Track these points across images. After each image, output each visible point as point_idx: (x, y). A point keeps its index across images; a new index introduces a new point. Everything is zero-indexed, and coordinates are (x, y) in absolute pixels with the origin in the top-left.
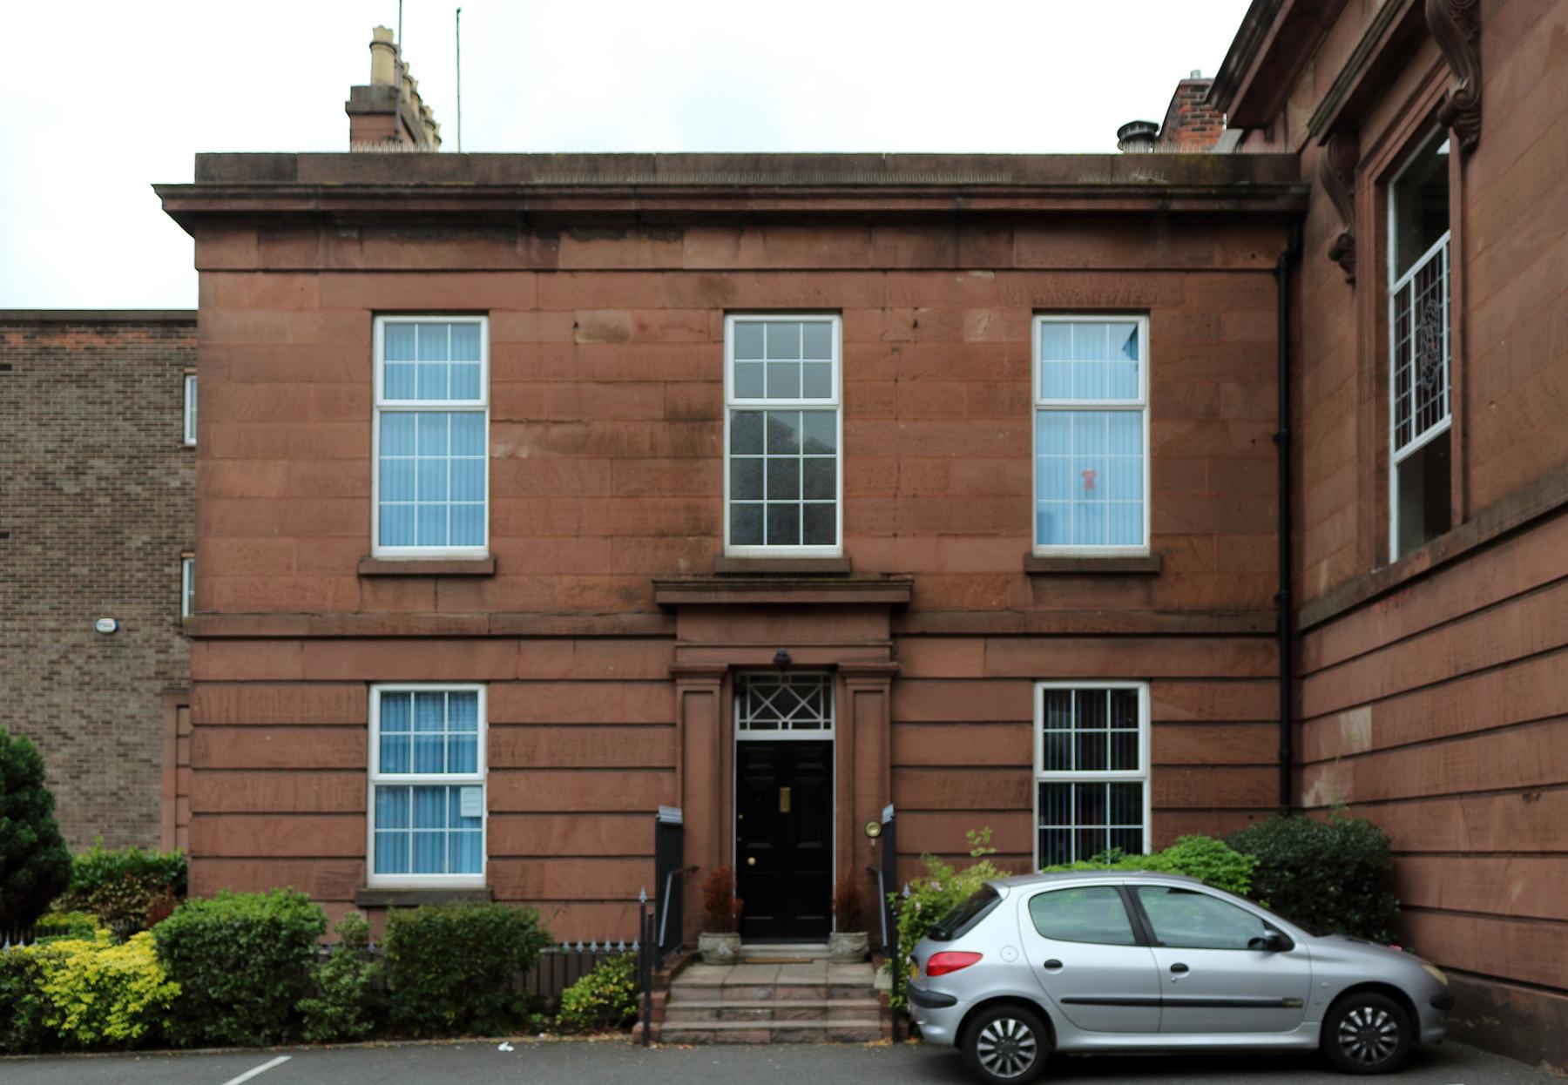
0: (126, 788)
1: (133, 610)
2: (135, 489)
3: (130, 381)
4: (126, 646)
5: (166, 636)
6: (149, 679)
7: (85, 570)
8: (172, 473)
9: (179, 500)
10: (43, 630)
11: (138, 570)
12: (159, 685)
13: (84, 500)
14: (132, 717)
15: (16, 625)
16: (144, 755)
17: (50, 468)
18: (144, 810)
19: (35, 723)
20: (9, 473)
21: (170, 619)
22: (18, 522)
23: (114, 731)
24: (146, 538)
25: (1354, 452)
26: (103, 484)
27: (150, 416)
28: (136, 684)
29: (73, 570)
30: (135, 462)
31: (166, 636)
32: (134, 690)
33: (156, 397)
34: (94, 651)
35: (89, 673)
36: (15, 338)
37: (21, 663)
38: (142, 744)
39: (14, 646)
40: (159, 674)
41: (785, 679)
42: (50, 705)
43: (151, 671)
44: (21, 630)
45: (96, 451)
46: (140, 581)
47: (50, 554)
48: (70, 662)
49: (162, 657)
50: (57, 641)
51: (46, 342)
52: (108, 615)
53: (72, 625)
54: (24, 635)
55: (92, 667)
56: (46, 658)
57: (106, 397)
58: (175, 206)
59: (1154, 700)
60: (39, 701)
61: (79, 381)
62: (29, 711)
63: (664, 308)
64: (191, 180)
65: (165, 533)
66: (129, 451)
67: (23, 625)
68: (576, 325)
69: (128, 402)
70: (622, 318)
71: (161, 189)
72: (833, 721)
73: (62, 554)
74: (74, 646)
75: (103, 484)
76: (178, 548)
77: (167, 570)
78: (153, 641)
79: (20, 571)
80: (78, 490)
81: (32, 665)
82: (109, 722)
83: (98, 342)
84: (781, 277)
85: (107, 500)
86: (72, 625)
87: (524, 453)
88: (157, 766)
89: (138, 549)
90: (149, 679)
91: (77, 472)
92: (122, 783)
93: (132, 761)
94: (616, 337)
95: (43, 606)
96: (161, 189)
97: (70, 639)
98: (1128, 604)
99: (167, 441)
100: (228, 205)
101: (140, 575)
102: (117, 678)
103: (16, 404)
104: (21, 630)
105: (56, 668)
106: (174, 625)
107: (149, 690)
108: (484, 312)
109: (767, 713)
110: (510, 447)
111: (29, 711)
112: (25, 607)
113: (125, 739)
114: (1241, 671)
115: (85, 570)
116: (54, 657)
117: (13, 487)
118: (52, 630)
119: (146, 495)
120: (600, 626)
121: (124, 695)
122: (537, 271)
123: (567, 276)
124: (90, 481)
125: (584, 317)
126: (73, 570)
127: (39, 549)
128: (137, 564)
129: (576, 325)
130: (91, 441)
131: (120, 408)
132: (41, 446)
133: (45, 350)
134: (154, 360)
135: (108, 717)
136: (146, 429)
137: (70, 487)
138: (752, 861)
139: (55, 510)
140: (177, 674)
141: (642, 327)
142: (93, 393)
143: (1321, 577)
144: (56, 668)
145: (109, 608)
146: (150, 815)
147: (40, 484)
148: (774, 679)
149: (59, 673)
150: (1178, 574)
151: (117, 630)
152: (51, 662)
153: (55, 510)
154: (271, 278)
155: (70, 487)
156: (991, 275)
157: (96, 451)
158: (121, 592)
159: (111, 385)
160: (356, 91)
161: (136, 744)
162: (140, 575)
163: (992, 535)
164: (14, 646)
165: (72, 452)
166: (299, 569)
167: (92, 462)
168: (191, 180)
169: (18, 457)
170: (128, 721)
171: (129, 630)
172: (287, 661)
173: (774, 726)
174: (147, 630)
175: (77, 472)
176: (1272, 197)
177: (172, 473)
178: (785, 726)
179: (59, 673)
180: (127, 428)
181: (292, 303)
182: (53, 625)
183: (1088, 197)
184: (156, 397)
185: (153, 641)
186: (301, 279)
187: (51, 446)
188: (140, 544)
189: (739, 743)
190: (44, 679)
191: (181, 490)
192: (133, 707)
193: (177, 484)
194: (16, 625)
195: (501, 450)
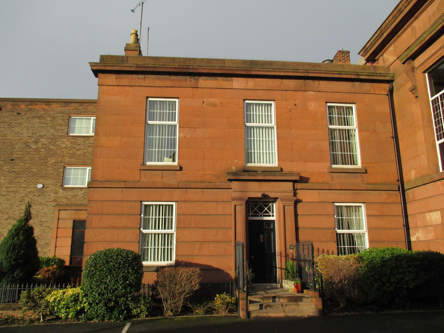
0: (41, 235)
1: (48, 182)
2: (52, 147)
3: (54, 118)
4: (45, 192)
5: (57, 189)
6: (51, 202)
7: (35, 170)
8: (63, 143)
9: (64, 150)
10: (21, 187)
11: (51, 170)
12: (54, 204)
13: (37, 150)
14: (45, 213)
15: (13, 186)
16: (47, 225)
17: (29, 141)
18: (46, 242)
19: (16, 215)
20: (16, 142)
21: (59, 184)
22: (17, 156)
23: (39, 217)
24: (54, 161)
25: (424, 140)
26: (43, 146)
27: (59, 127)
28: (47, 203)
29: (32, 170)
30: (53, 140)
31: (57, 189)
32: (46, 205)
33: (61, 122)
34: (35, 193)
35: (33, 200)
36: (23, 106)
37: (13, 197)
38: (47, 221)
39: (12, 192)
40: (54, 200)
41: (261, 202)
42: (21, 210)
43: (52, 200)
44: (15, 187)
45: (42, 137)
46: (51, 173)
47: (26, 165)
48: (28, 197)
49: (56, 195)
50: (25, 190)
51: (31, 107)
52: (41, 183)
53: (30, 186)
54: (15, 189)
55: (35, 198)
56: (21, 195)
57: (47, 122)
58: (94, 68)
59: (367, 209)
60: (18, 208)
61: (39, 118)
62: (14, 211)
63: (227, 98)
64: (98, 61)
65: (60, 160)
66: (52, 137)
67: (15, 186)
68: (203, 102)
69: (52, 124)
70: (216, 101)
71: (89, 63)
72: (275, 214)
73: (29, 165)
74: (30, 192)
75: (43, 146)
76: (63, 164)
77: (59, 170)
78: (53, 191)
79: (16, 170)
80: (36, 147)
81: (17, 198)
82: (38, 215)
83: (46, 107)
84: (259, 91)
85: (44, 150)
86: (30, 186)
87: (188, 136)
88: (51, 228)
89: (51, 164)
90: (51, 202)
91: (36, 142)
92: (40, 233)
93: (44, 226)
94: (214, 105)
95: (22, 180)
96: (89, 63)
97: (29, 190)
98: (358, 181)
99: (63, 134)
100: (103, 69)
101: (51, 172)
102: (42, 201)
103: (21, 124)
104: (15, 187)
105: (24, 198)
106: (60, 186)
107: (50, 205)
108: (178, 98)
109: (256, 212)
110: (185, 134)
111: (14, 211)
112: (17, 180)
113: (42, 220)
114: (389, 201)
115: (35, 170)
116: (23, 195)
117: (17, 146)
118: (23, 187)
119: (55, 149)
120: (211, 185)
121: (43, 206)
122: (193, 88)
123: (200, 89)
124: (40, 145)
125: (205, 100)
126: (32, 170)
127: (23, 164)
128: (51, 168)
129: (203, 102)
130: (41, 134)
131: (50, 125)
132: (26, 135)
133: (31, 109)
134: (61, 113)
135: (38, 213)
136: (57, 131)
137: (34, 147)
138: (253, 257)
139: (29, 153)
140: (60, 200)
141: (221, 103)
142: (43, 121)
143: (410, 175)
144: (24, 198)
145: (41, 181)
146: (47, 243)
147: (25, 146)
148: (258, 202)
149: (24, 200)
150: (370, 174)
151: (43, 187)
152: (23, 197)
153: (29, 153)
154: (119, 88)
155: (34, 147)
156: (314, 93)
157: (42, 137)
158: (45, 177)
159: (48, 119)
160: (127, 45)
161: (46, 221)
162: (51, 172)
163: (319, 162)
164: (12, 192)
165: (35, 137)
166: (122, 168)
167: (41, 140)
168: (98, 61)
169: (19, 138)
170: (43, 214)
171: (47, 187)
172: (117, 194)
173: (258, 216)
174: (52, 187)
175: (36, 142)
176: (385, 76)
177: (63, 143)
178: (261, 216)
179: (24, 200)
180: (52, 130)
181: (128, 93)
182: (24, 186)
183: (339, 74)
184: (61, 122)
185: (53, 191)
186: (127, 88)
187: (29, 135)
188: (52, 163)
189: (249, 220)
190: (20, 202)
191: (66, 148)
192: (46, 210)
193: (64, 146)
194: (13, 186)
195: (182, 135)
